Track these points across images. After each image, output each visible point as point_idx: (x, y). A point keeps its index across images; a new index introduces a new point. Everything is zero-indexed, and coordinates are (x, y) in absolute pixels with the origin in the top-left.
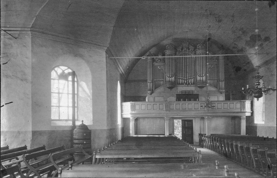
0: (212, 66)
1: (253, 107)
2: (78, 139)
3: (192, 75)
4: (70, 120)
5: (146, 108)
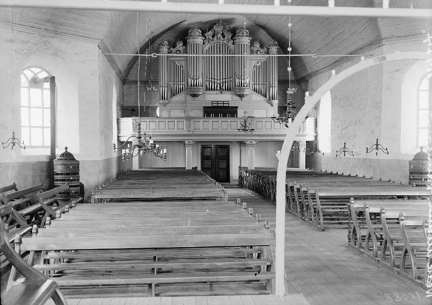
0: (258, 63)
1: (51, 119)
2: (62, 174)
3: (224, 78)
4: (46, 147)
5: (157, 127)
